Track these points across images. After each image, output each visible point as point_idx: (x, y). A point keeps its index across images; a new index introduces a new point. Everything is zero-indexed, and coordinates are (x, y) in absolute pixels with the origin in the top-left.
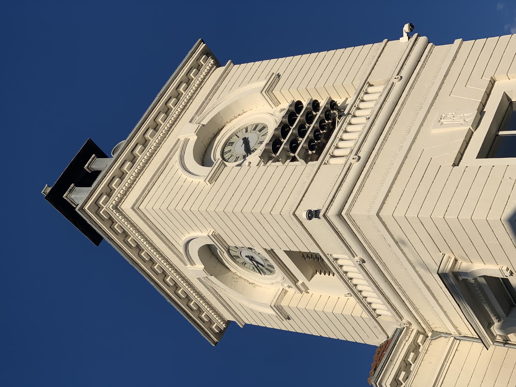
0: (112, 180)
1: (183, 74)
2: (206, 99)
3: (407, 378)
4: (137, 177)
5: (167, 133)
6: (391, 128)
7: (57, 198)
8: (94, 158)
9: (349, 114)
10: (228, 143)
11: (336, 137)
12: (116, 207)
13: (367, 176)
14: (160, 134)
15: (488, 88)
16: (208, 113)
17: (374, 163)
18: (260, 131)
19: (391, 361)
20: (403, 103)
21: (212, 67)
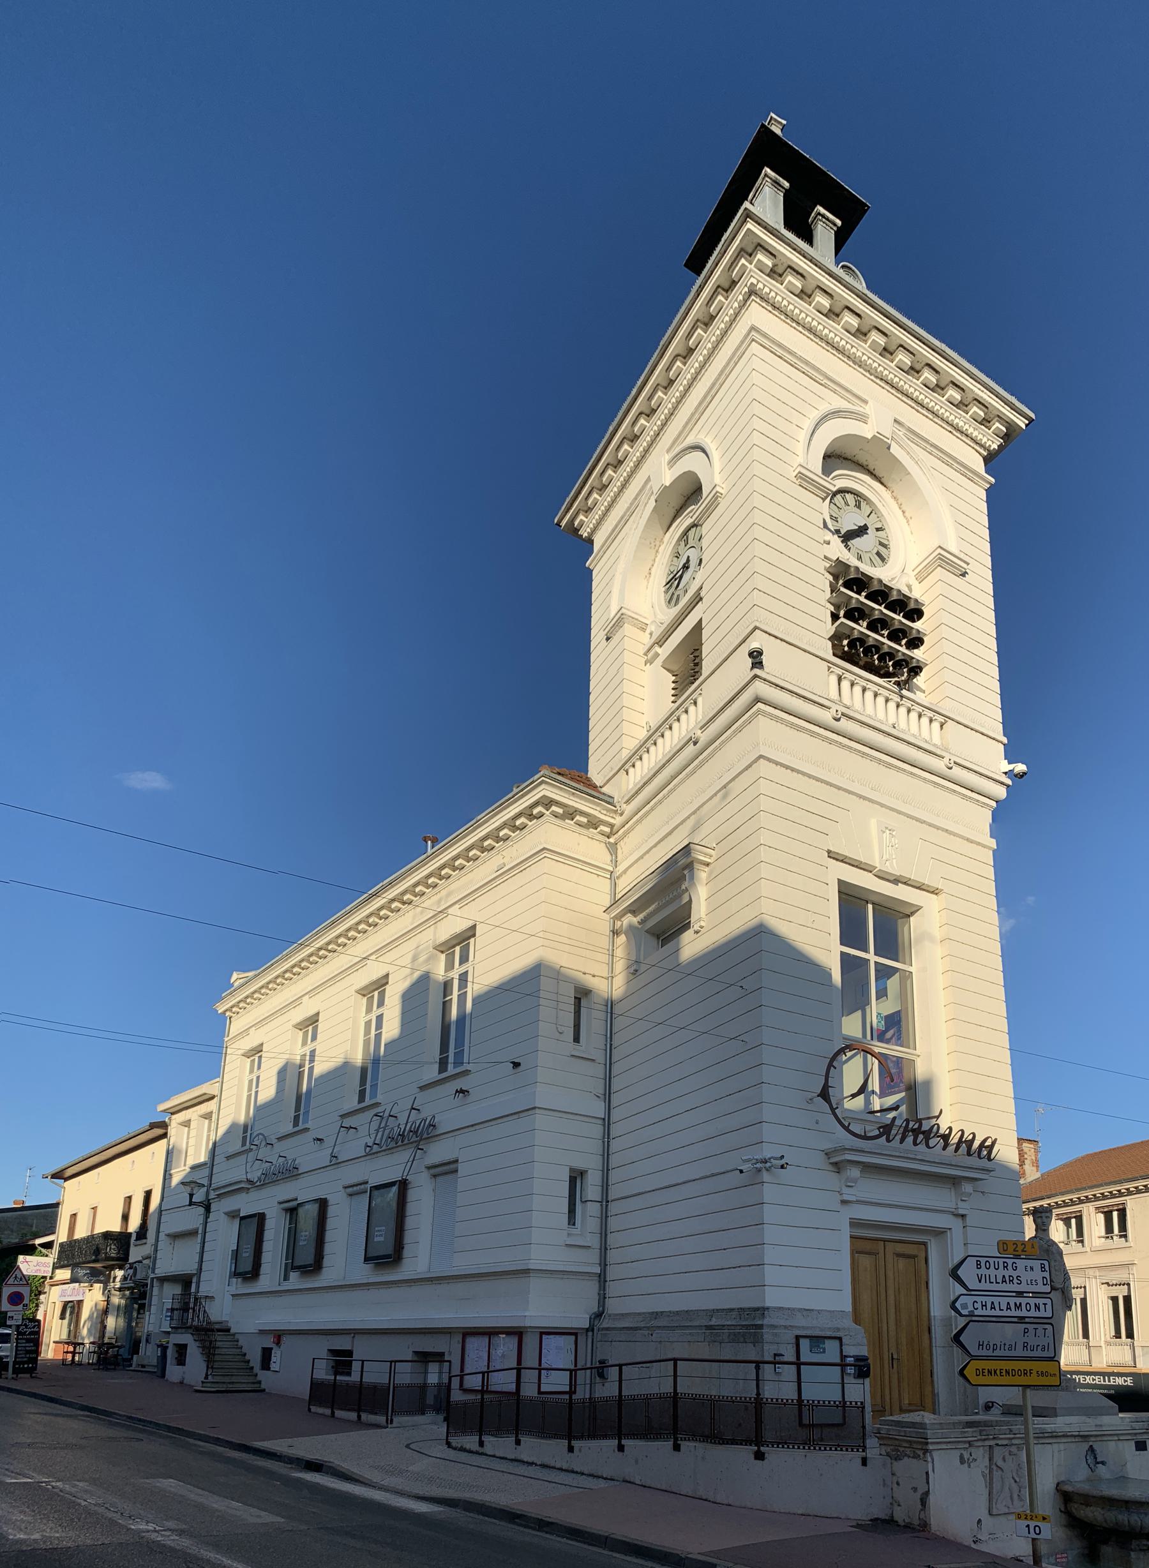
2: (933, 445)
7: (768, 151)
9: (902, 697)
12: (752, 292)
20: (914, 775)
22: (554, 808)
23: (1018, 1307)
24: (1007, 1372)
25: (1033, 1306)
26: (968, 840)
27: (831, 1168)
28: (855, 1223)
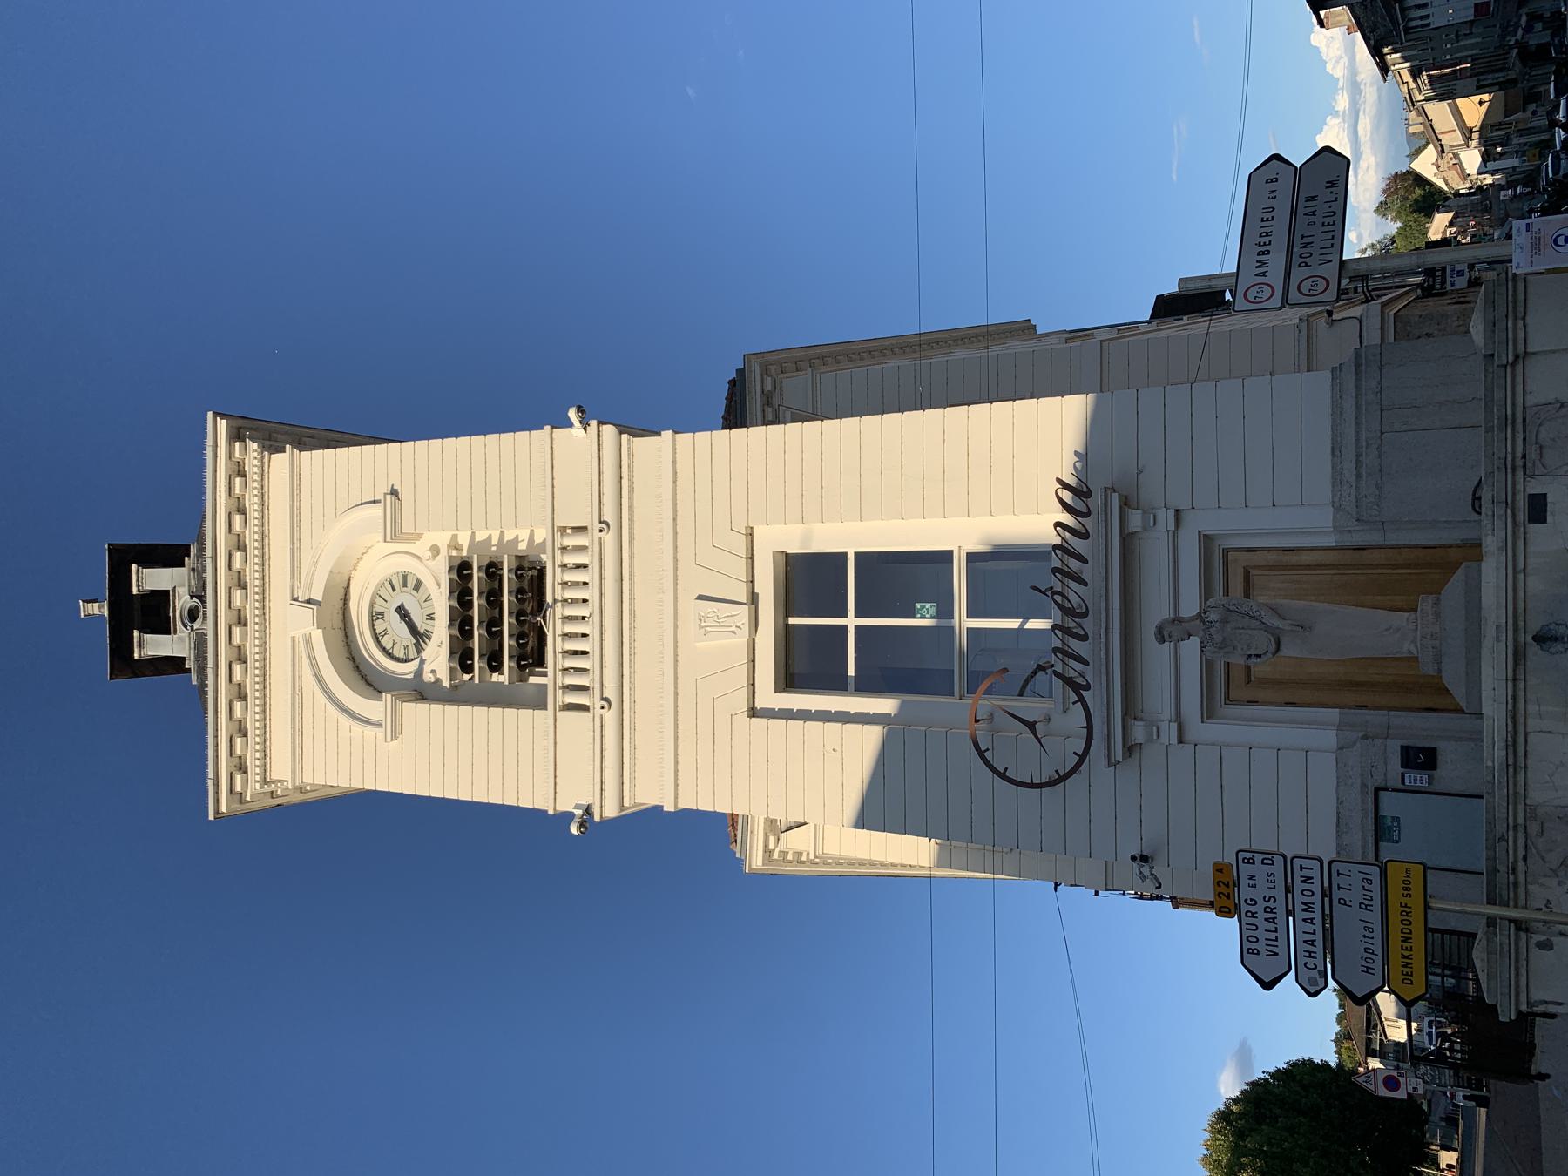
7: (123, 662)
9: (555, 601)
12: (265, 782)
17: (633, 702)
18: (405, 585)
23: (1308, 907)
24: (1406, 940)
25: (1306, 886)
27: (1136, 755)
28: (1209, 712)
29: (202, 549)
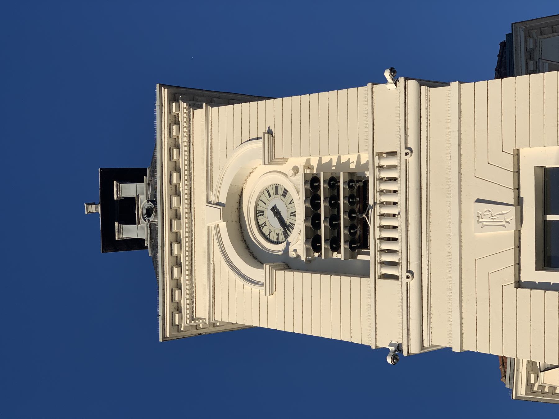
0: (172, 295)
1: (166, 140)
2: (208, 166)
3: (538, 377)
4: (192, 279)
5: (192, 216)
6: (428, 223)
7: (110, 243)
8: (117, 185)
9: (375, 203)
10: (259, 213)
11: (375, 239)
12: (192, 318)
13: (429, 293)
14: (184, 220)
15: (514, 165)
16: (220, 187)
19: (517, 370)
21: (189, 112)
22: (532, 381)
26: (460, 118)
29: (154, 171)
